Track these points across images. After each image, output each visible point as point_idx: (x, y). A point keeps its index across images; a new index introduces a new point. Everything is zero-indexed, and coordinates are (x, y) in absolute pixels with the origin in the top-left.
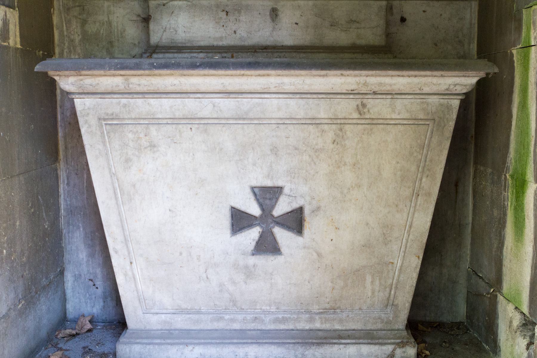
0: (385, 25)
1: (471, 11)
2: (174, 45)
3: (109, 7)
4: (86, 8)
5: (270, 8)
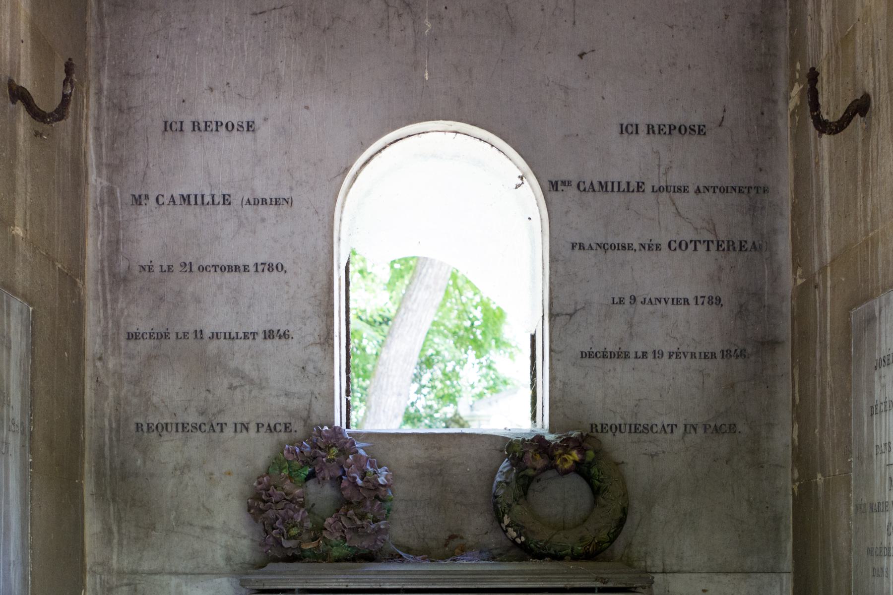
1: (781, 589)
3: (178, 586)
4: (139, 587)
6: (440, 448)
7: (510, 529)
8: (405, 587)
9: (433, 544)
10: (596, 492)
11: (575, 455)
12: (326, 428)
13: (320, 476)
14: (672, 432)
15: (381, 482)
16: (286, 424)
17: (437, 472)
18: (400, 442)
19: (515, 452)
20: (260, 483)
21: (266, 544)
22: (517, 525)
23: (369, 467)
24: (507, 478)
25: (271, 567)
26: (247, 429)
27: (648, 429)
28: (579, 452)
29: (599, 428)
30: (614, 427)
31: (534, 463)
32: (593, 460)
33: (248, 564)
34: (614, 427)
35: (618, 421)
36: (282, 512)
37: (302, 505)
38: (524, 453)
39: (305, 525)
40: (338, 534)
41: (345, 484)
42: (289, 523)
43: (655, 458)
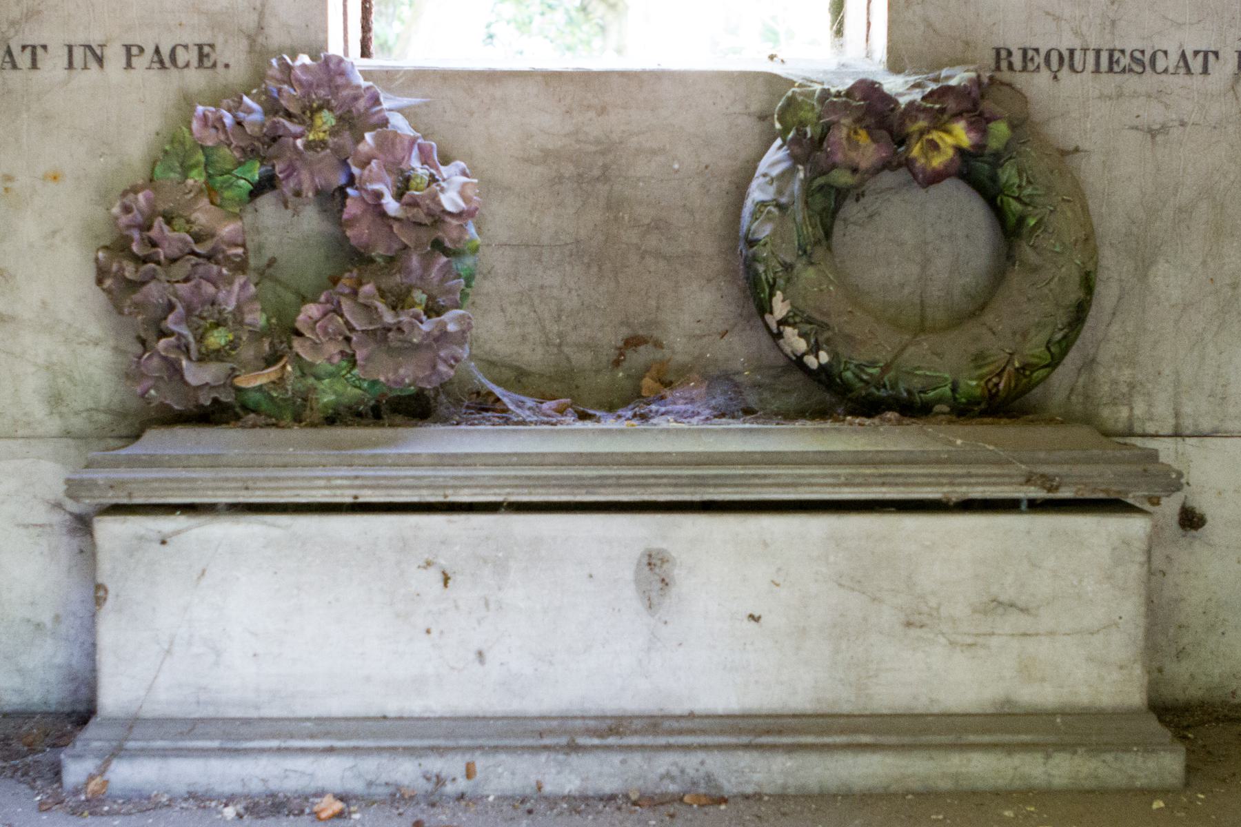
0: (1142, 622)
2: (210, 712)
5: (637, 551)
6: (603, 111)
7: (789, 331)
8: (513, 499)
9: (583, 359)
10: (1010, 229)
11: (961, 134)
12: (304, 59)
13: (288, 187)
14: (1205, 71)
15: (449, 207)
16: (200, 47)
17: (596, 172)
18: (498, 93)
19: (802, 124)
20: (127, 209)
21: (143, 375)
22: (809, 321)
23: (415, 163)
24: (780, 192)
25: (156, 441)
26: (100, 60)
27: (1144, 62)
28: (971, 126)
29: (1017, 60)
30: (1054, 58)
31: (853, 154)
32: (1007, 146)
33: (108, 411)
34: (1054, 58)
35: (1066, 42)
36: (183, 289)
37: (240, 266)
38: (828, 128)
39: (249, 318)
40: (333, 349)
41: (353, 208)
42: (205, 316)
43: (1159, 138)
